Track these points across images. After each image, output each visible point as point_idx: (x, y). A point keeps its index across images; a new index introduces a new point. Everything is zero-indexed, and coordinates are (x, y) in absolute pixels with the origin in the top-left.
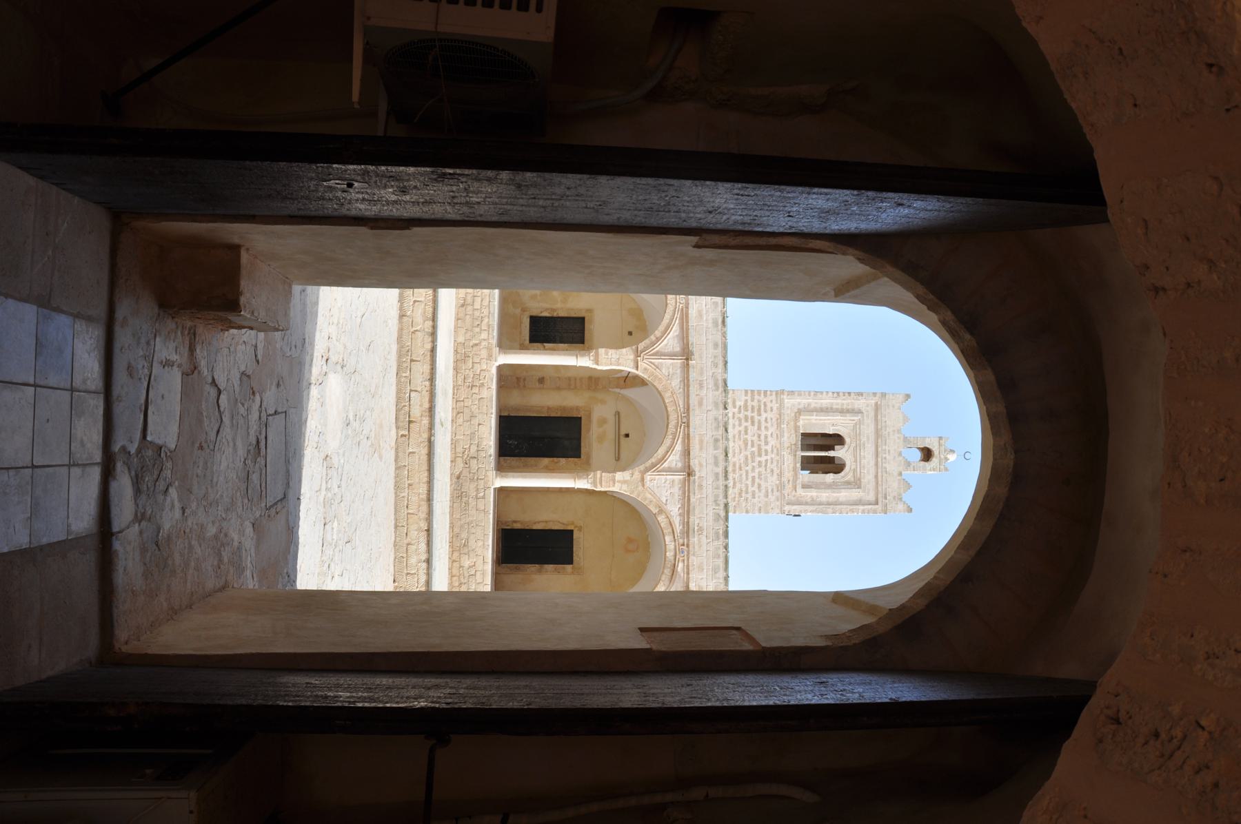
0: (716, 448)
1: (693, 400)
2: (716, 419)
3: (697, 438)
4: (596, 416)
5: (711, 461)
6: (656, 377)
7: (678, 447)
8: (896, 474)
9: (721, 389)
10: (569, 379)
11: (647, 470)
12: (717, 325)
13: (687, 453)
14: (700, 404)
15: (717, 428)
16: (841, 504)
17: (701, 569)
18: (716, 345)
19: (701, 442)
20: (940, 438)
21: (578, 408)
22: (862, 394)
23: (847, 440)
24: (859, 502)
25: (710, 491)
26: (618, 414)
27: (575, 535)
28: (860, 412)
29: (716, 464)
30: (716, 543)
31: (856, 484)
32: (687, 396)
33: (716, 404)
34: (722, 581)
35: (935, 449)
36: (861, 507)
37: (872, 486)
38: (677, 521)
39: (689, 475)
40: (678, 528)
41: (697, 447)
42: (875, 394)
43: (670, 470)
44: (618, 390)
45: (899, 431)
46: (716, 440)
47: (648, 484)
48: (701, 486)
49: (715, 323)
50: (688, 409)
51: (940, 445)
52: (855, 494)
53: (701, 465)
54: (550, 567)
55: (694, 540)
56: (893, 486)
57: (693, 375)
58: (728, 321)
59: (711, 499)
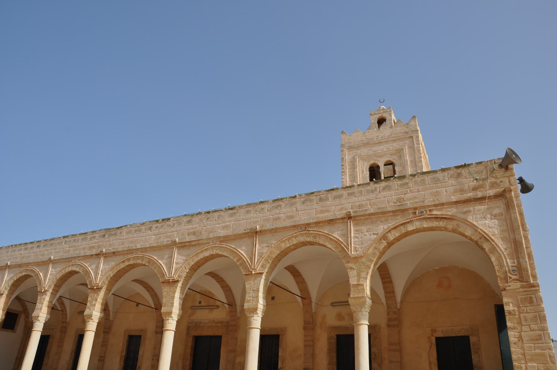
0: (327, 199)
1: (288, 223)
2: (304, 202)
3: (321, 215)
4: (336, 323)
5: (338, 201)
6: (268, 256)
7: (326, 230)
8: (391, 130)
9: (280, 203)
10: (305, 346)
11: (347, 255)
12: (235, 213)
13: (331, 222)
14: (291, 217)
15: (311, 201)
16: (415, 158)
17: (437, 194)
18: (248, 212)
19: (322, 212)
20: (371, 115)
21: (329, 338)
22: (343, 158)
23: (372, 162)
24: (412, 148)
25: (363, 198)
26: (333, 304)
27: (440, 335)
28: (354, 158)
29: (340, 196)
30: (411, 185)
31: (400, 152)
32: (285, 228)
33: (292, 205)
34: (446, 174)
35: (377, 117)
36: (416, 145)
37: (401, 143)
38: (392, 224)
39: (350, 217)
40: (400, 220)
41: (326, 214)
42: (342, 151)
43: (346, 235)
44: (313, 305)
45: (364, 133)
46: (321, 200)
47: (359, 253)
48: (360, 206)
49: (231, 215)
50: (295, 227)
51: (375, 114)
52: (407, 151)
53: (342, 209)
54: (474, 358)
55: (409, 204)
56: (399, 130)
57: (268, 226)
58: (231, 206)
59: (372, 196)
